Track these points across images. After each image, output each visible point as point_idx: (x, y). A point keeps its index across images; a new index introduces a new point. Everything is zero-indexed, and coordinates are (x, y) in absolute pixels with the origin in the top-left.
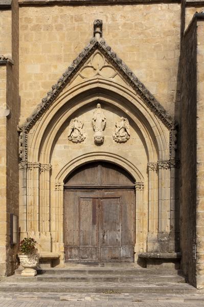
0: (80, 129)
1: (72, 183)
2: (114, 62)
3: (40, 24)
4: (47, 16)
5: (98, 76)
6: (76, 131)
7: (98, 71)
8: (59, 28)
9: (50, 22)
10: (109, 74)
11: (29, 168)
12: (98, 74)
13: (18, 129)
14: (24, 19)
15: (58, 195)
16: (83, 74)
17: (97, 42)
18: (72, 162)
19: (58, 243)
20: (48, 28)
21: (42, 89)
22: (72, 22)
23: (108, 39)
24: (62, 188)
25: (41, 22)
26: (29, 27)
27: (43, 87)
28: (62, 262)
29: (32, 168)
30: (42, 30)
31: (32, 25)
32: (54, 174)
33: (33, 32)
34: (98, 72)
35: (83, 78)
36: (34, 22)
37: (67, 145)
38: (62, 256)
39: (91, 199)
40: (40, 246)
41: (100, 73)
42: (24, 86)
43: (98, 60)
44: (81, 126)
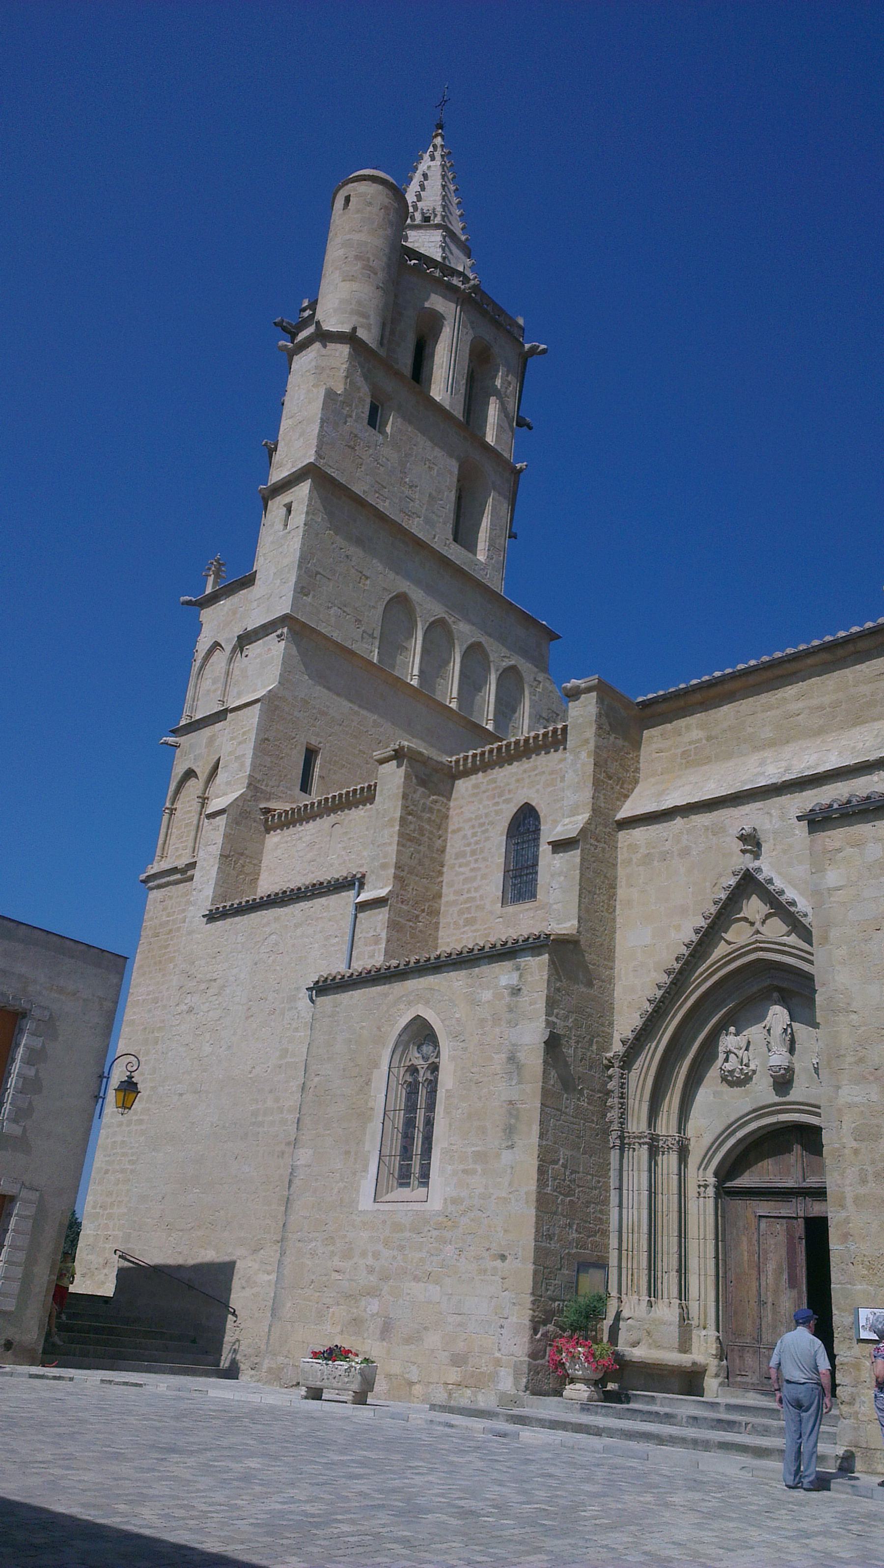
0: (740, 1053)
1: (745, 1181)
2: (780, 908)
3: (652, 851)
4: (665, 834)
5: (759, 937)
6: (732, 1056)
7: (758, 925)
8: (685, 853)
9: (668, 846)
10: (775, 930)
11: (629, 1144)
12: (758, 932)
13: (605, 1062)
14: (625, 849)
15: (702, 1211)
16: (728, 936)
17: (748, 870)
18: (730, 1129)
19: (704, 1333)
20: (664, 857)
21: (655, 974)
22: (707, 838)
23: (767, 868)
24: (711, 1191)
25: (654, 848)
26: (635, 860)
27: (655, 971)
28: (711, 1384)
29: (637, 1146)
30: (655, 862)
31: (639, 856)
32: (693, 1160)
33: (641, 868)
34: (754, 932)
35: (729, 943)
36: (643, 850)
37: (719, 1089)
38: (713, 1365)
39: (784, 1221)
40: (648, 1333)
41: (761, 929)
42: (623, 972)
43: (754, 907)
44: (744, 1045)
